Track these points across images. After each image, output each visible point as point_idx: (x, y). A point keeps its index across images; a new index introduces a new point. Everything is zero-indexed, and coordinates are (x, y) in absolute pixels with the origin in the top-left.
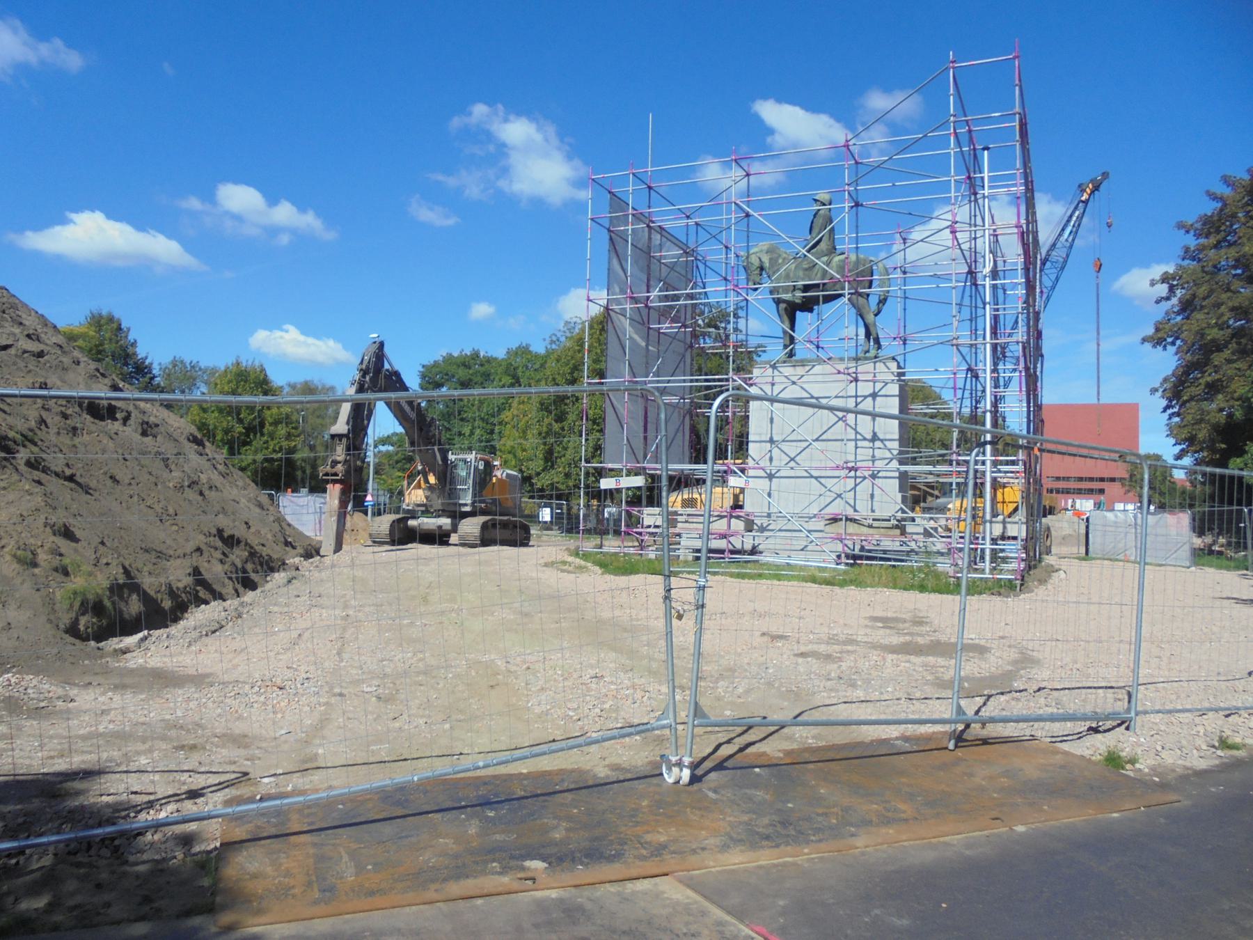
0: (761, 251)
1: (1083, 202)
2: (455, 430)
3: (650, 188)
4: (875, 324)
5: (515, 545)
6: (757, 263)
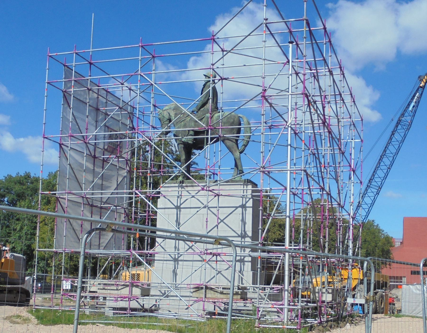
0: (170, 108)
1: (421, 87)
2: (12, 227)
3: (91, 64)
4: (240, 158)
5: (15, 305)
6: (167, 117)
